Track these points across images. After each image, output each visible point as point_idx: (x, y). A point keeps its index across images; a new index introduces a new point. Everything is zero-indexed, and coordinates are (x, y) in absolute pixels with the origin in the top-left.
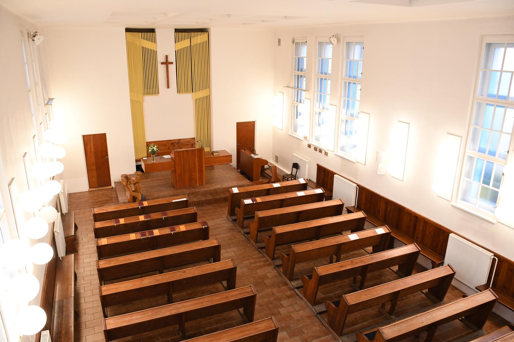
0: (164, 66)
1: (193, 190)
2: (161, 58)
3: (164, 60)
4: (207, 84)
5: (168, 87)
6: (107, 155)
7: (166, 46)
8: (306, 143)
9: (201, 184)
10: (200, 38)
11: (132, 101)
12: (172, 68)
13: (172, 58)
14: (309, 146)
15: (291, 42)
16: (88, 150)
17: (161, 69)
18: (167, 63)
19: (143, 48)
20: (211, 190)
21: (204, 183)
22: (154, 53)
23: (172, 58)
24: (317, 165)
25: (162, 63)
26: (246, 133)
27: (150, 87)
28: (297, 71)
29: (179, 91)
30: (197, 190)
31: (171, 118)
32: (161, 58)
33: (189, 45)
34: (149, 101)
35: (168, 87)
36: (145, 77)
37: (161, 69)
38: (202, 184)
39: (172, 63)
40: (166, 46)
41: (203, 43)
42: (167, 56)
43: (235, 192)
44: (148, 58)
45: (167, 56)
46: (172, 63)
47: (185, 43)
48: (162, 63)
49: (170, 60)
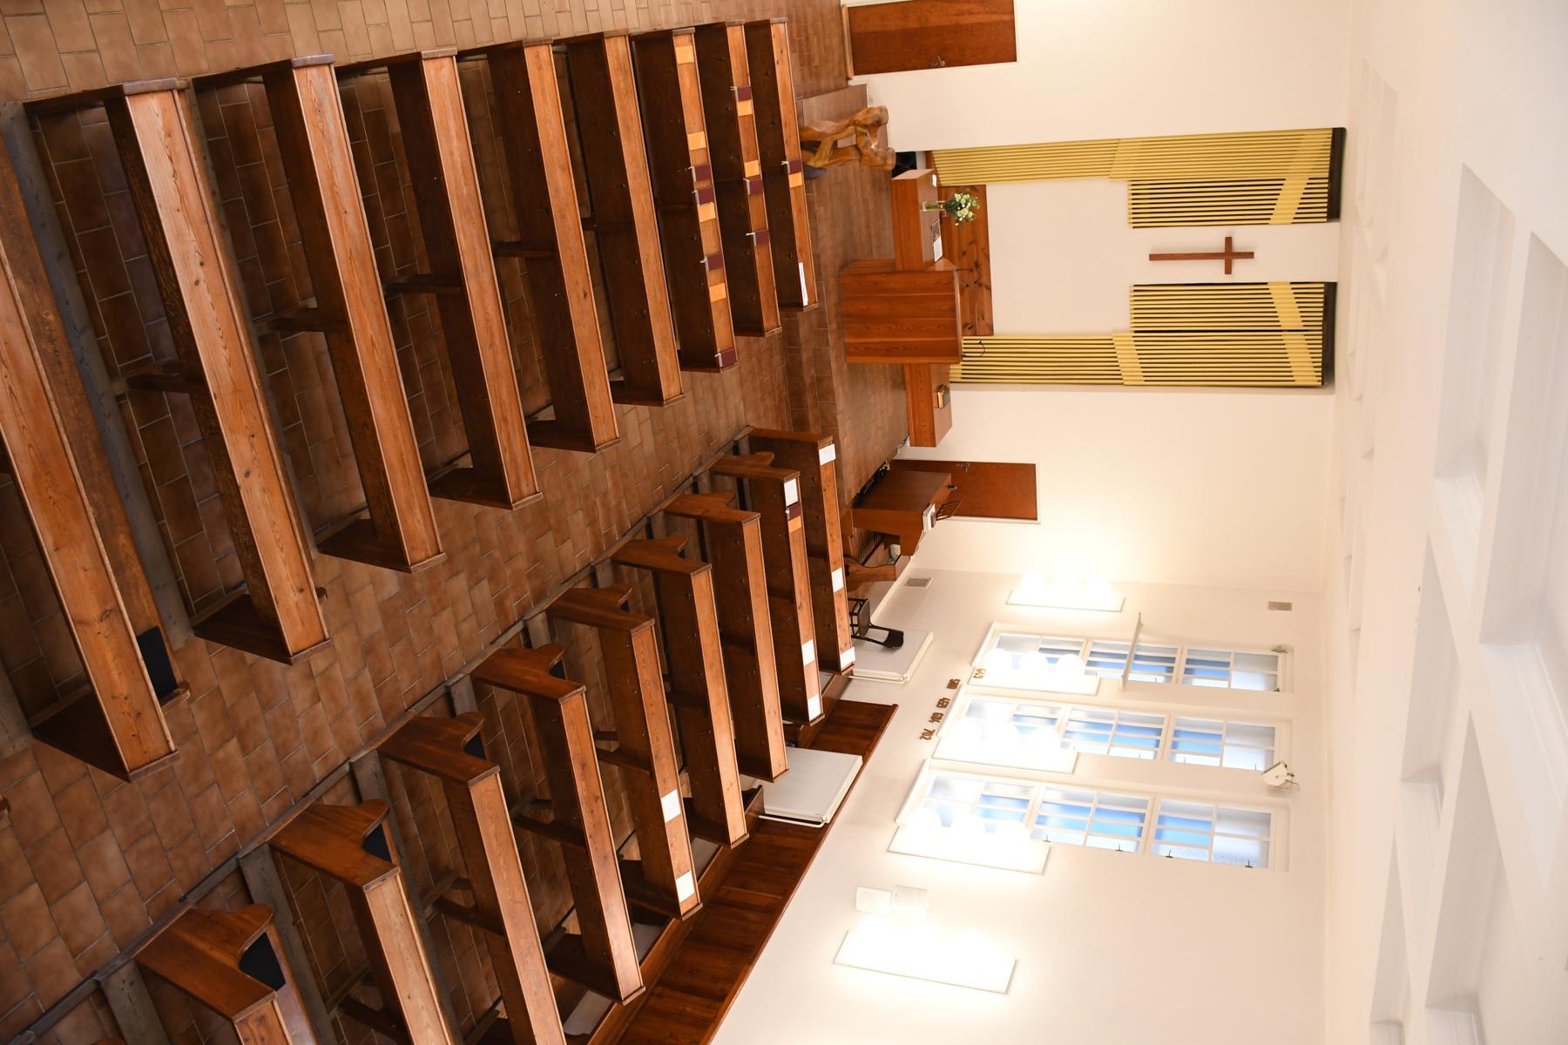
0: (1220, 246)
1: (834, 326)
2: (1244, 236)
3: (1238, 246)
4: (1158, 376)
5: (1153, 257)
7: (1284, 253)
8: (962, 673)
9: (850, 351)
10: (1302, 357)
11: (1111, 147)
12: (1212, 272)
13: (1243, 271)
14: (953, 684)
17: (1210, 237)
18: (1229, 255)
19: (1278, 184)
20: (830, 378)
21: (852, 359)
22: (1261, 216)
23: (1243, 271)
24: (895, 706)
26: (1002, 491)
27: (1156, 202)
28: (1186, 656)
29: (1139, 289)
30: (831, 339)
32: (1244, 236)
34: (1114, 196)
35: (1153, 257)
36: (1190, 187)
37: (1210, 237)
38: (849, 354)
39: (1228, 271)
40: (1284, 253)
41: (1286, 367)
42: (1250, 255)
43: (821, 452)
44: (1252, 199)
45: (1250, 255)
46: (1228, 271)
47: (1289, 313)
48: (1229, 240)
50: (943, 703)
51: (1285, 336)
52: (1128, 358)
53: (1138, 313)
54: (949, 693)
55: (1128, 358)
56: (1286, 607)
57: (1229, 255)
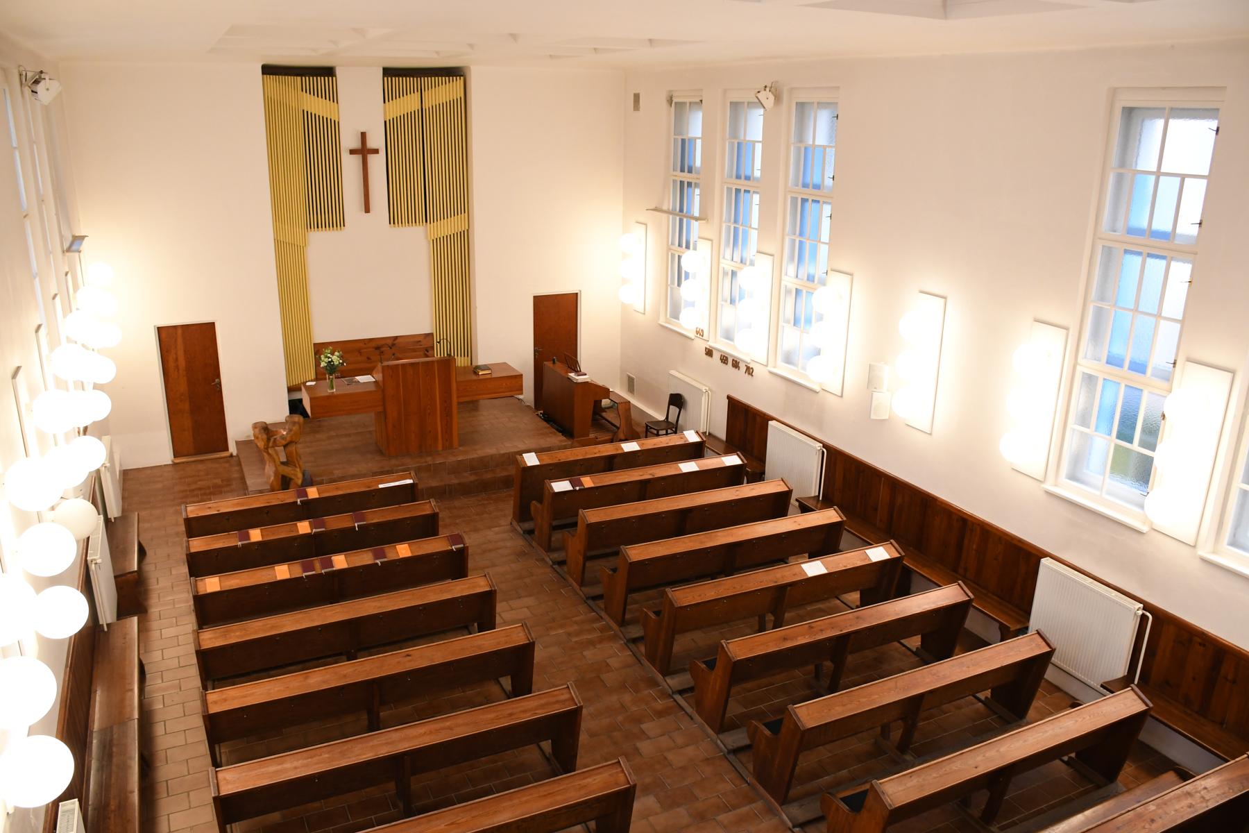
0: (357, 159)
1: (429, 459)
2: (349, 140)
4: (460, 202)
5: (367, 210)
6: (218, 376)
7: (361, 110)
8: (700, 346)
10: (444, 92)
11: (280, 245)
12: (377, 164)
13: (376, 140)
14: (709, 353)
15: (664, 104)
16: (171, 364)
17: (350, 165)
18: (363, 151)
21: (455, 443)
22: (333, 127)
23: (376, 140)
24: (728, 397)
25: (352, 152)
26: (556, 320)
27: (324, 210)
28: (678, 173)
29: (393, 220)
30: (439, 460)
31: (375, 286)
32: (349, 140)
33: (417, 106)
34: (321, 246)
35: (367, 210)
36: (310, 184)
37: (350, 165)
38: (451, 447)
39: (376, 151)
40: (361, 110)
41: (451, 104)
42: (363, 135)
43: (529, 464)
44: (319, 135)
45: (363, 135)
46: (376, 151)
47: (408, 104)
48: (352, 152)
49: (371, 144)
50: (724, 360)
51: (426, 106)
52: (448, 227)
53: (412, 220)
54: (716, 356)
55: (448, 227)
56: (637, 97)
57: (363, 151)
